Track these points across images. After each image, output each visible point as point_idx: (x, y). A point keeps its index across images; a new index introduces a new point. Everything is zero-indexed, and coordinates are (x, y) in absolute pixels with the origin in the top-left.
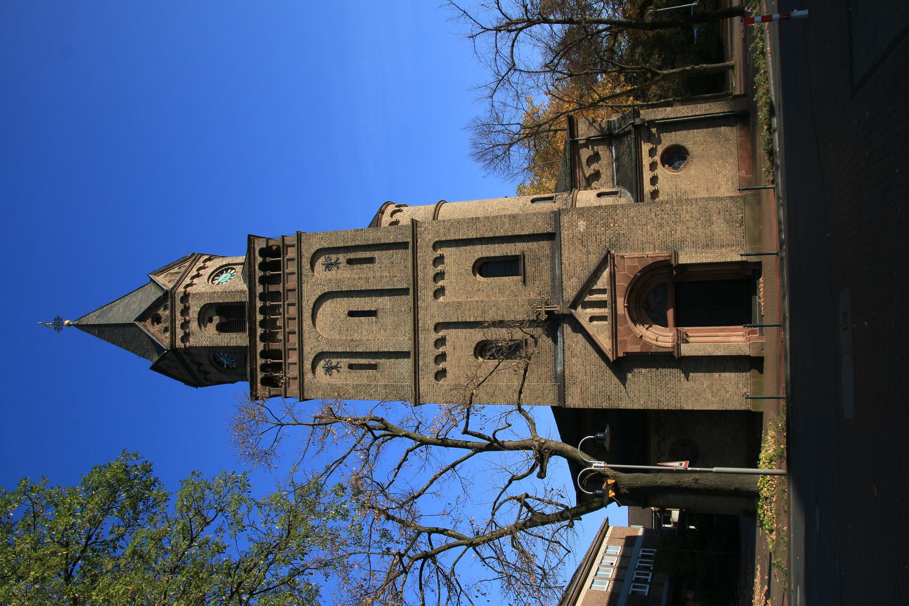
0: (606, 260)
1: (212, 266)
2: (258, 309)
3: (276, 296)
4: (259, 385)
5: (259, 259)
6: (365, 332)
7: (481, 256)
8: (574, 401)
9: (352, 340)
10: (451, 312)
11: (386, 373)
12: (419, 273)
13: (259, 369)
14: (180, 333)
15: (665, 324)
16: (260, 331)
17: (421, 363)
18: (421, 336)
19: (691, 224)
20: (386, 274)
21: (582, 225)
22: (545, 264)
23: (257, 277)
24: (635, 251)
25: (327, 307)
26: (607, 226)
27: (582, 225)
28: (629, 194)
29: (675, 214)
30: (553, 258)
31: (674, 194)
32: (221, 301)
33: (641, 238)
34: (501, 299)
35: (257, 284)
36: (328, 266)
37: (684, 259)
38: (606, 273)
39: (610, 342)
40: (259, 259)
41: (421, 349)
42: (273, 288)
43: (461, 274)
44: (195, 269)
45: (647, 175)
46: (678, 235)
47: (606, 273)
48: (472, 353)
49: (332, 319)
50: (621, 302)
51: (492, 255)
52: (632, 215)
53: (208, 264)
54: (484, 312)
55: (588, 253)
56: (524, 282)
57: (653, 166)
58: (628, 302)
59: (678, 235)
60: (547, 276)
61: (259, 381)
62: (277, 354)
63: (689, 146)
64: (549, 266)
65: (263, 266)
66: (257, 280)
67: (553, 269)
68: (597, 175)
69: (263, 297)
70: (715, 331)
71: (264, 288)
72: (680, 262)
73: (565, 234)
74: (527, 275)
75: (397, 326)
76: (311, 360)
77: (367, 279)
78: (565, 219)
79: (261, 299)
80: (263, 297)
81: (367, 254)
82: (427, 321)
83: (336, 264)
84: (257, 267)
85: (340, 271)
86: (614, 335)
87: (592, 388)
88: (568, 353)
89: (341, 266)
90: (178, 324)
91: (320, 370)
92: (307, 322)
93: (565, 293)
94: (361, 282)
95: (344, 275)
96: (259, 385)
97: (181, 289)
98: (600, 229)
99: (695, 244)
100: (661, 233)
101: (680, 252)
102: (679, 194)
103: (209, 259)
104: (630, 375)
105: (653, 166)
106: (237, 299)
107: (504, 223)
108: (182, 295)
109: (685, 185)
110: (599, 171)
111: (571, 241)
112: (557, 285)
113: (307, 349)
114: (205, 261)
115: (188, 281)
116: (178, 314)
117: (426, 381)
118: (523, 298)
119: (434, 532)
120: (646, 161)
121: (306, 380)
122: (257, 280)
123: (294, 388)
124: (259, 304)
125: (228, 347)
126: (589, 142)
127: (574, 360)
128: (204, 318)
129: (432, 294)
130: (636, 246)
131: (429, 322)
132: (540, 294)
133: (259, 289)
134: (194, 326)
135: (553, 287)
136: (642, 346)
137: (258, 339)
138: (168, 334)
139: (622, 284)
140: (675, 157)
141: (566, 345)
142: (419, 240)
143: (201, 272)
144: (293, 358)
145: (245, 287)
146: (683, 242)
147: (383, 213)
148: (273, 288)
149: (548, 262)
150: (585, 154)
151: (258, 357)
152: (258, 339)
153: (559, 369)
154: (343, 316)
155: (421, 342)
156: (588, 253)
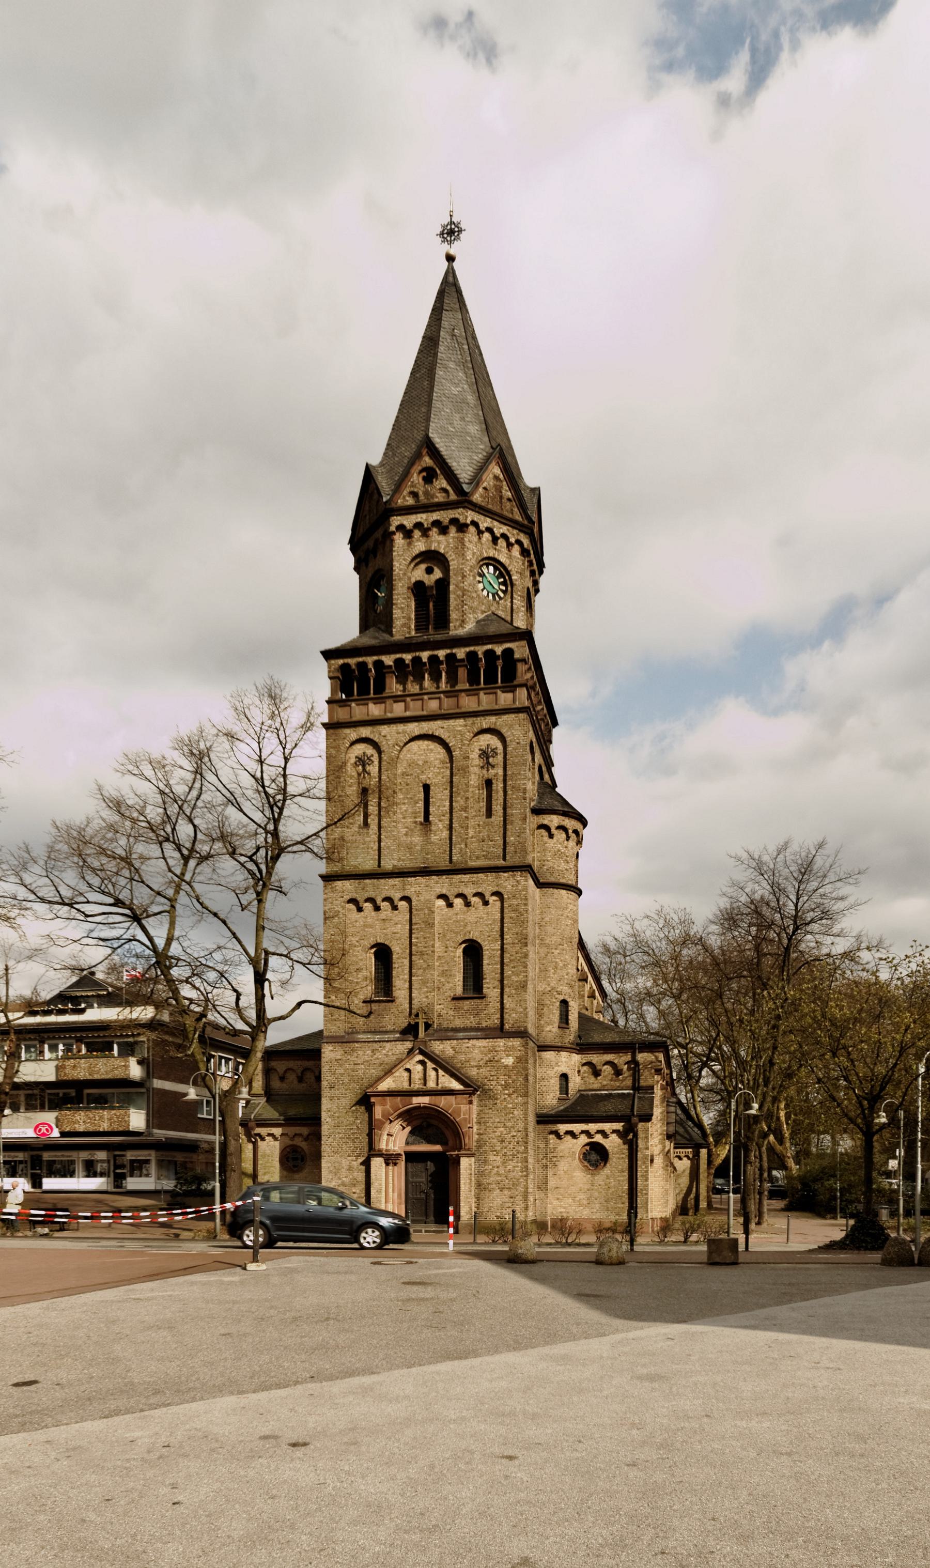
0: (471, 1088)
1: (510, 557)
2: (436, 653)
3: (453, 679)
4: (341, 662)
5: (499, 649)
6: (404, 808)
7: (485, 948)
8: (329, 1053)
9: (394, 792)
10: (422, 916)
11: (358, 838)
12: (468, 876)
13: (360, 659)
14: (409, 521)
15: (407, 1143)
16: (408, 657)
17: (367, 881)
18: (396, 881)
19: (501, 1171)
20: (471, 832)
21: (509, 1061)
22: (471, 1021)
23: (476, 648)
24: (478, 1115)
25: (438, 752)
26: (506, 1086)
27: (509, 1061)
28: (562, 1108)
29: (513, 1155)
30: (477, 1029)
31: (555, 1154)
32: (452, 587)
33: (492, 1120)
34: (436, 973)
35: (468, 649)
36: (486, 755)
37: (465, 1162)
38: (456, 1085)
39: (386, 1089)
40: (499, 649)
41: (382, 881)
42: (462, 673)
43: (465, 926)
44: (504, 529)
45: (577, 1127)
46: (492, 1158)
47: (456, 1085)
48: (379, 941)
49: (420, 763)
50: (424, 1100)
51: (485, 962)
52: (516, 1112)
53: (516, 550)
54: (422, 954)
55: (479, 1067)
56: (455, 999)
57: (587, 1133)
58: (424, 1107)
59: (492, 1158)
60: (458, 1023)
61: (346, 661)
62: (380, 686)
63: (607, 1171)
64: (469, 1025)
65: (490, 654)
66: (472, 648)
67: (465, 1029)
68: (596, 1073)
69: (451, 658)
70: (400, 1190)
71: (462, 660)
72: (462, 1159)
73: (501, 1042)
74: (461, 1002)
75: (410, 848)
76: (372, 737)
77: (465, 809)
78: (516, 1042)
79: (447, 656)
80: (451, 658)
81: (497, 808)
82: (415, 886)
83: (488, 765)
84: (489, 647)
85: (477, 770)
86: (391, 1094)
87: (340, 1073)
88: (376, 1046)
89: (485, 771)
90: (421, 517)
91: (360, 749)
92: (414, 728)
93: (438, 1042)
94: (462, 802)
95: (473, 776)
96: (341, 662)
97: (470, 516)
98: (502, 1079)
99: (480, 1174)
100: (495, 1141)
101: (473, 1159)
102: (555, 1159)
103: (524, 552)
104: (363, 1108)
105: (587, 1133)
106: (454, 615)
107: (518, 975)
108: (462, 520)
109: (563, 1165)
110: (600, 1075)
111: (493, 1050)
112: (447, 1034)
113: (385, 729)
114: (518, 542)
115: (485, 522)
116: (435, 516)
117: (347, 887)
118: (435, 997)
119: (171, 917)
120: (592, 1127)
121: (347, 731)
122: (472, 648)
123: (342, 714)
124: (442, 654)
125: (392, 604)
126: (634, 1065)
127: (369, 1052)
128: (432, 558)
129: (444, 892)
130: (483, 1116)
131: (413, 889)
132: (440, 1015)
133: (461, 653)
134: (420, 546)
135: (447, 1030)
136: (379, 1120)
137: (398, 656)
138: (410, 501)
139: (443, 1102)
140: (596, 1155)
141: (385, 1044)
142: (506, 874)
143: (502, 543)
144: (375, 710)
145: (470, 627)
146: (486, 1162)
147: (565, 814)
148: (462, 673)
149: (474, 1024)
150: (622, 1060)
151: (375, 658)
152: (398, 656)
153: (361, 1037)
154: (423, 777)
155: (391, 881)
156: (479, 1067)
